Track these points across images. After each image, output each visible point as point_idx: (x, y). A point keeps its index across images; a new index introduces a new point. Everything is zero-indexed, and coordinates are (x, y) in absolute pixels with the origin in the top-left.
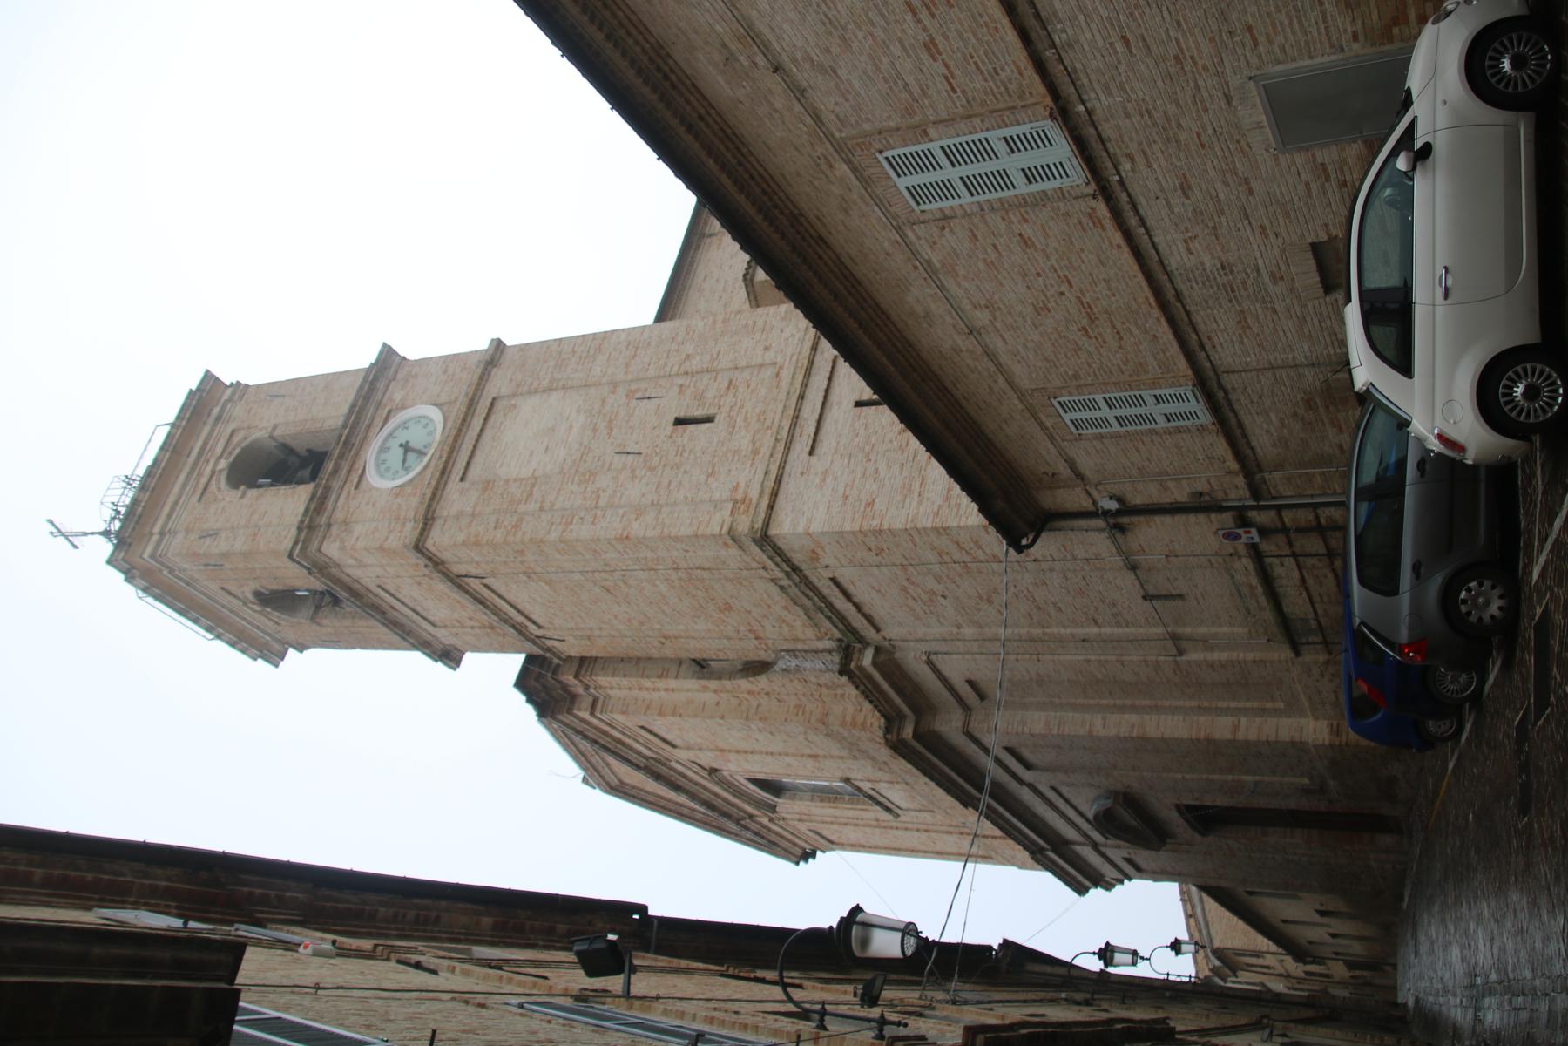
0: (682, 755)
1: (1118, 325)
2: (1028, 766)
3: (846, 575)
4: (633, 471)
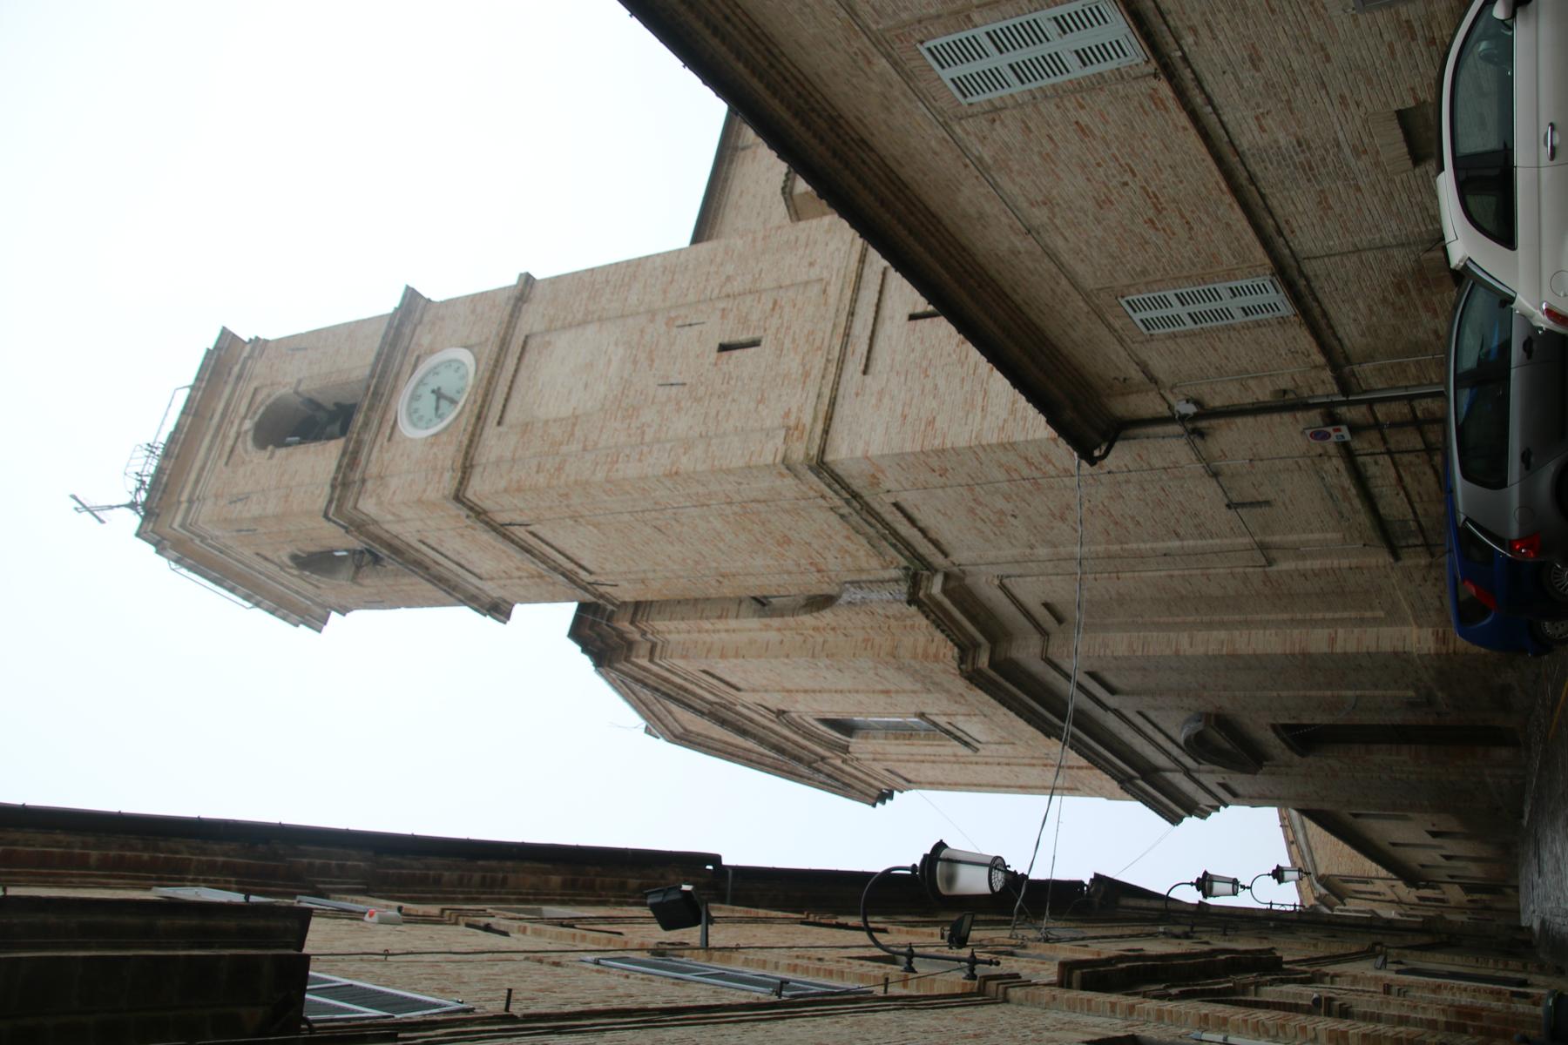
1: (1188, 215)
2: (1112, 691)
3: (909, 499)
4: (678, 403)
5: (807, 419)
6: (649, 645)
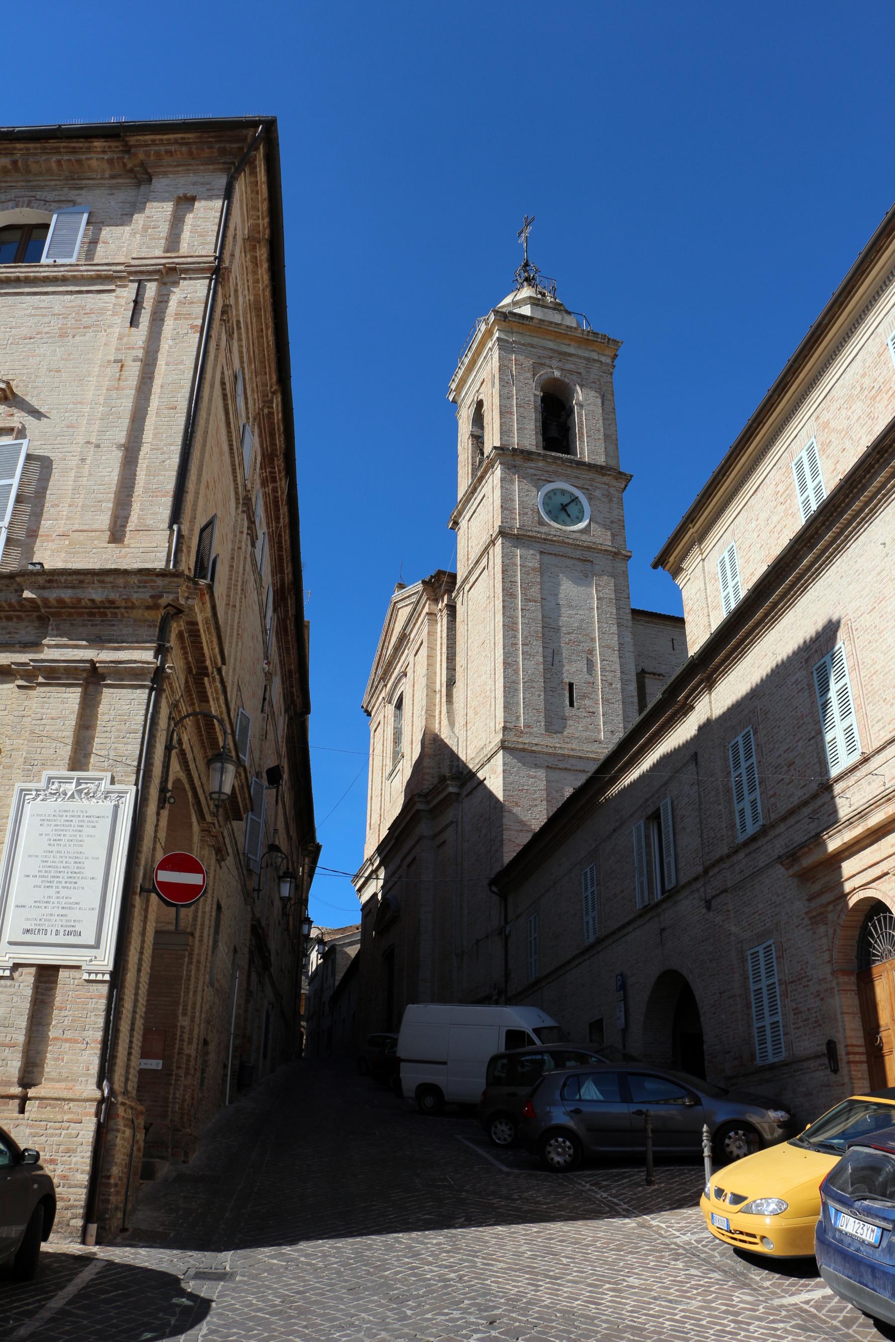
2: (409, 866)
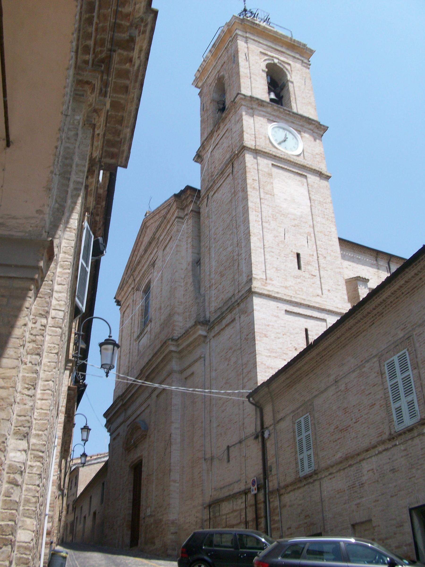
0: (160, 253)
1: (339, 441)
3: (237, 325)
4: (277, 236)
5: (269, 288)
6: (183, 216)
